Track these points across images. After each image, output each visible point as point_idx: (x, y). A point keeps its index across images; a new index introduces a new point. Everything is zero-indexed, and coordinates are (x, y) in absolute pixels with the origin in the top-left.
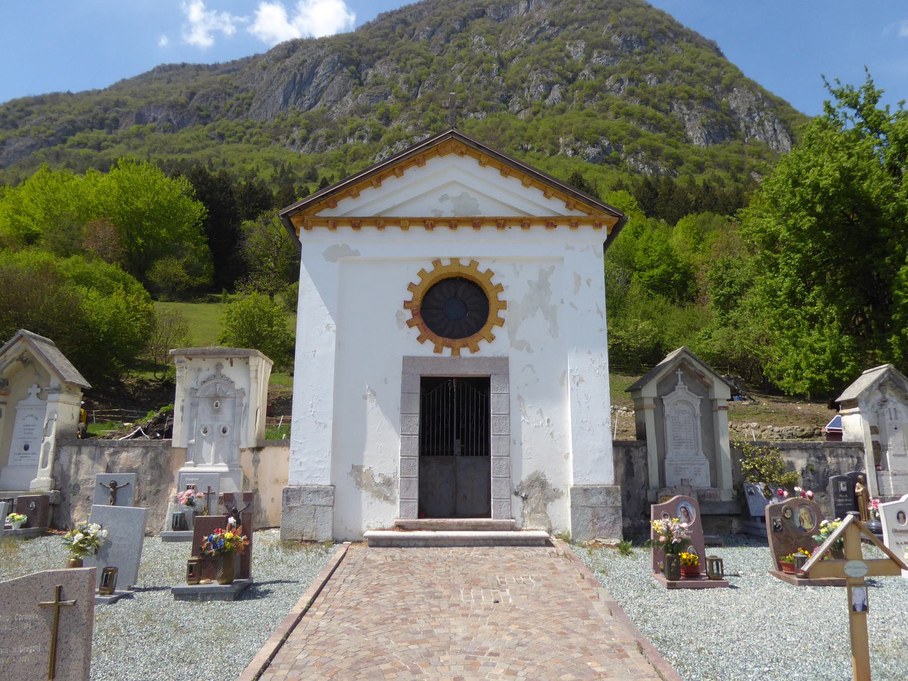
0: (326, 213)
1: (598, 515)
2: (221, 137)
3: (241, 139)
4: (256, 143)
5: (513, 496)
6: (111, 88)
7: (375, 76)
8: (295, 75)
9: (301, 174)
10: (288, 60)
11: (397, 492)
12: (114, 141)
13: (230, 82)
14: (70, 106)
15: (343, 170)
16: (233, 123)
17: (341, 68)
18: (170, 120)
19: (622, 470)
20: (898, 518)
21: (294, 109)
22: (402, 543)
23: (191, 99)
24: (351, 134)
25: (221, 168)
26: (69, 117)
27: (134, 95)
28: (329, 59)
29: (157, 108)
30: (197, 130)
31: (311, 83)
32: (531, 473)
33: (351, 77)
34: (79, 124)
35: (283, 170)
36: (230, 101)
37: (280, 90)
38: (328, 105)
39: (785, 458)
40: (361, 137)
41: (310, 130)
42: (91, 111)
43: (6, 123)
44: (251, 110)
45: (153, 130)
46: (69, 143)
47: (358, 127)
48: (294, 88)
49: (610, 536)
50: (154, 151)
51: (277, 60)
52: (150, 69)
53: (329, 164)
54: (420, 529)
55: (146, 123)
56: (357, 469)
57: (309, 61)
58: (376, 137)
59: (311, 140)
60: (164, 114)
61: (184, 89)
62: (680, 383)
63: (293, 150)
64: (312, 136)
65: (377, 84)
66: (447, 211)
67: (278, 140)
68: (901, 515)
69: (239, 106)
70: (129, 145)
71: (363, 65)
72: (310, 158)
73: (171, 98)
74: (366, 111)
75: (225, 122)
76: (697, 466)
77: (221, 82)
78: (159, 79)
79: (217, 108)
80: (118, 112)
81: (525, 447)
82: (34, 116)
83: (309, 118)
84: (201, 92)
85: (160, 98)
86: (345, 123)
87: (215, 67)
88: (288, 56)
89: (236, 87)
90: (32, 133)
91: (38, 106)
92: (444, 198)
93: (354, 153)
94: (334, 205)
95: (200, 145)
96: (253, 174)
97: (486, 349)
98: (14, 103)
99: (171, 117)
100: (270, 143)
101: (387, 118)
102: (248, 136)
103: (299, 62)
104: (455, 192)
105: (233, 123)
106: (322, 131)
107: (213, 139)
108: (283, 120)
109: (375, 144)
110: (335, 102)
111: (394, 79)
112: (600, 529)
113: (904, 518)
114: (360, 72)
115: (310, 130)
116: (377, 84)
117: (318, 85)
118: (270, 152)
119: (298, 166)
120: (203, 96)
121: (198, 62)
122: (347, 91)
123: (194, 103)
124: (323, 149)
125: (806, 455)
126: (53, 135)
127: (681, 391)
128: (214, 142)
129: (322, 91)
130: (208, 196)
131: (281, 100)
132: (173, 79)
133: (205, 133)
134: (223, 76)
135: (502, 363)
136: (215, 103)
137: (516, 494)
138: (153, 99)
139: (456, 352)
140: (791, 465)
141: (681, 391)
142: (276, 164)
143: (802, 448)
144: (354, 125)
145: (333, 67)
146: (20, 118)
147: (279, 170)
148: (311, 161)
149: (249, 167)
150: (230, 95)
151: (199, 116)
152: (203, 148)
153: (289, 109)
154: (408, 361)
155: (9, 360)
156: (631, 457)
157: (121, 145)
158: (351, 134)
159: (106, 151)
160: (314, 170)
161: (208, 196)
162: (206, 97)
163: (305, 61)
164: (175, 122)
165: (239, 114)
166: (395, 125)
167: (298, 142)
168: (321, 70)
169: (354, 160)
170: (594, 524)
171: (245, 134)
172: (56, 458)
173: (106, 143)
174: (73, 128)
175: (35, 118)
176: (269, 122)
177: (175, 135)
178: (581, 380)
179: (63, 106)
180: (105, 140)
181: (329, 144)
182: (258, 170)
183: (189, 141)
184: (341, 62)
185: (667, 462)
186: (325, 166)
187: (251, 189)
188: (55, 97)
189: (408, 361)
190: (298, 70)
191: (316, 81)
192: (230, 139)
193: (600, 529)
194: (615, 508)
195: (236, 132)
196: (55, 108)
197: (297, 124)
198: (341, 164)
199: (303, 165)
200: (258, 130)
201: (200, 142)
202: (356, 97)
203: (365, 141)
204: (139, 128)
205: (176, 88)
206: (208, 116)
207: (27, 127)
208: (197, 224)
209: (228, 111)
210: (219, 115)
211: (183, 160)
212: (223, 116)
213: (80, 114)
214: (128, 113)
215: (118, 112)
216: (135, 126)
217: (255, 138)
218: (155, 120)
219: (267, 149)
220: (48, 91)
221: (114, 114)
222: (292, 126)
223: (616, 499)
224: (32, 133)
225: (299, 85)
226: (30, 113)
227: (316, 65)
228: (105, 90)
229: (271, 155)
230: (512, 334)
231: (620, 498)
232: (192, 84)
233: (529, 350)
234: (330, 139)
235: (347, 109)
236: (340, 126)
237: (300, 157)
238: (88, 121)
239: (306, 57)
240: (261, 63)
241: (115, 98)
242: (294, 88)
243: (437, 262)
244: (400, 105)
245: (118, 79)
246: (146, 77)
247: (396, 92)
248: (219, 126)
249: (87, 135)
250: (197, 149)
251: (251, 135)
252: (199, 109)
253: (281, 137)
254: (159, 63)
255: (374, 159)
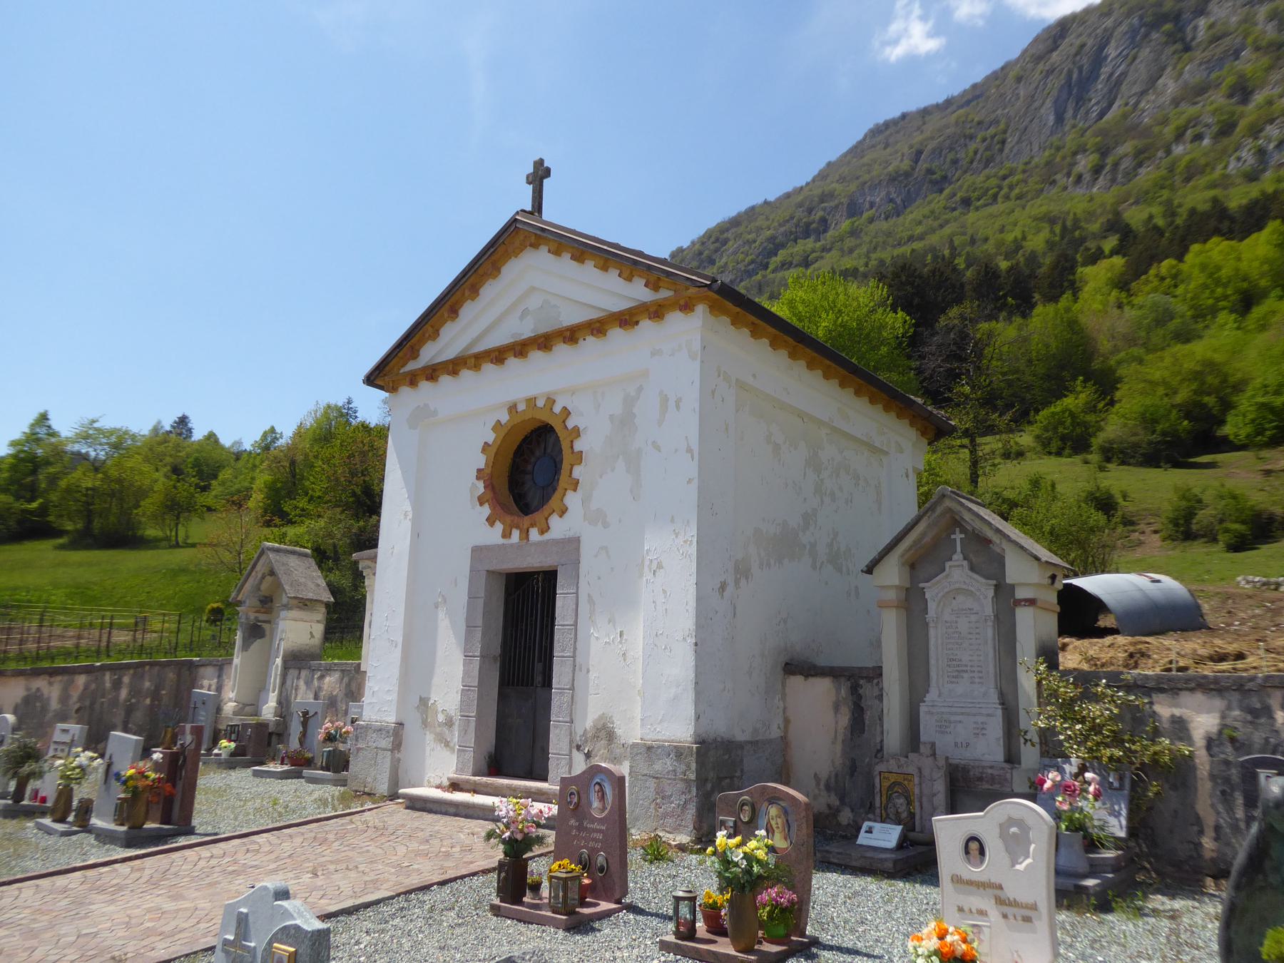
0: (412, 366)
1: (663, 791)
2: (966, 202)
3: (995, 197)
4: (1019, 197)
5: (574, 751)
6: (814, 180)
7: (1211, 26)
8: (1070, 73)
9: (1095, 227)
10: (1055, 54)
11: (455, 738)
12: (824, 249)
13: (970, 117)
14: (767, 219)
15: (1169, 203)
16: (982, 178)
17: (1146, 35)
18: (891, 201)
19: (845, 719)
20: (967, 852)
21: (1074, 126)
22: (434, 807)
23: (916, 162)
24: (1179, 137)
25: (968, 249)
26: (769, 233)
27: (842, 179)
28: (1123, 28)
29: (873, 187)
30: (930, 202)
31: (1098, 77)
32: (596, 717)
33: (1166, 43)
34: (780, 239)
35: (1064, 228)
36: (972, 146)
37: (1049, 103)
38: (1132, 102)
39: (1164, 709)
40: (1198, 137)
41: (1104, 152)
42: (792, 218)
43: (703, 261)
44: (1006, 150)
45: (871, 220)
46: (771, 267)
47: (1189, 121)
48: (1070, 94)
49: (676, 829)
50: (875, 248)
51: (1038, 59)
52: (860, 137)
53: (1143, 198)
54: (475, 792)
55: (861, 214)
56: (424, 702)
57: (1090, 42)
58: (1226, 129)
59: (1108, 168)
60: (883, 194)
61: (906, 150)
62: (958, 556)
63: (1079, 191)
64: (1110, 160)
65: (1216, 39)
66: (526, 330)
67: (1054, 182)
68: (974, 846)
69: (987, 149)
70: (842, 250)
71: (1186, 16)
72: (1109, 198)
73: (890, 168)
74: (1201, 90)
75: (969, 179)
76: (980, 719)
77: (957, 123)
78: (873, 146)
79: (955, 162)
80: (824, 209)
81: (592, 675)
82: (730, 243)
83: (1103, 133)
84: (929, 147)
85: (874, 173)
86: (1165, 121)
87: (949, 102)
88: (1055, 47)
89: (979, 123)
90: (731, 265)
91: (733, 230)
92: (525, 313)
93: (1188, 167)
94: (415, 354)
95: (936, 224)
96: (1018, 246)
97: (559, 527)
98: (709, 234)
99: (893, 195)
100: (1042, 190)
101: (1243, 91)
102: (1005, 190)
103: (1073, 50)
104: (534, 303)
105: (982, 178)
106: (1127, 148)
107: (954, 209)
108: (1058, 149)
109: (1226, 141)
110: (1143, 93)
111: (1248, 20)
112: (665, 816)
113: (982, 852)
114: (1181, 30)
115: (1104, 152)
116: (1216, 39)
117: (1111, 75)
118: (1039, 207)
119: (1091, 215)
120: (933, 151)
121: (922, 105)
122: (1163, 69)
123: (923, 165)
124: (1131, 175)
125: (1219, 703)
126: (752, 262)
127: (957, 572)
128: (956, 213)
129: (1119, 83)
130: (916, 301)
131: (1052, 118)
132: (891, 140)
133: (942, 203)
134: (961, 111)
135: (573, 544)
136: (951, 156)
137: (578, 748)
138: (867, 177)
139: (525, 535)
140: (1180, 728)
141: (957, 572)
142: (1052, 221)
143: (1211, 687)
144: (1181, 121)
145: (1133, 38)
146: (716, 251)
147: (1058, 229)
148: (1112, 201)
149: (1010, 237)
150: (972, 137)
151: (931, 182)
152: (941, 226)
153: (1067, 128)
154: (478, 552)
155: (260, 575)
156: (860, 697)
157: (834, 252)
158: (1179, 137)
159: (816, 265)
160: (1117, 214)
161: (916, 301)
162: (938, 152)
163: (1083, 46)
164: (899, 201)
165: (988, 162)
166: (1259, 98)
167: (1087, 177)
168: (1112, 51)
169: (1188, 180)
170: (658, 806)
171: (1000, 188)
172: (283, 683)
173: (814, 255)
174: (775, 246)
175: (732, 246)
176: (1036, 160)
177: (901, 218)
178: (660, 566)
179: (761, 222)
180: (813, 251)
181: (1140, 165)
182: (1024, 238)
183: (920, 223)
184: (1145, 25)
185: (923, 709)
186: (1136, 203)
187: (987, 273)
188: (752, 212)
189: (478, 552)
190: (1074, 63)
191: (1105, 71)
192: (979, 203)
193: (665, 816)
194: (687, 781)
195: (988, 190)
196: (752, 226)
197: (1082, 149)
198: (1166, 194)
199: (1099, 211)
200: (1019, 177)
201: (936, 219)
202: (1181, 74)
203: (1206, 142)
204: (853, 223)
205: (896, 152)
206: (945, 178)
207: (724, 260)
208: (901, 343)
209: (972, 162)
210: (959, 172)
211: (913, 250)
212: (965, 172)
213: (780, 225)
214: (837, 207)
215: (824, 209)
216: (848, 222)
217: (1017, 191)
218: (872, 205)
219: (1038, 201)
220: (743, 207)
221: (820, 213)
222: (1075, 154)
223: (688, 766)
224: (731, 265)
225: (1076, 90)
226: (725, 242)
227: (1102, 47)
228: (808, 184)
229: (1044, 209)
230: (585, 501)
231: (694, 766)
232: (917, 138)
233: (606, 525)
234: (1141, 156)
235: (1166, 98)
236: (1156, 129)
237: (1091, 199)
238: (791, 233)
239: (1083, 39)
240: (1012, 74)
241: (820, 191)
242: (1070, 94)
243: (512, 408)
244: (1265, 61)
245: (822, 165)
246: (857, 151)
247: (1255, 41)
248: (961, 187)
249: (790, 251)
250: (933, 231)
251: (1011, 187)
252: (930, 172)
253: (1058, 177)
254: (870, 125)
255: (1226, 167)
